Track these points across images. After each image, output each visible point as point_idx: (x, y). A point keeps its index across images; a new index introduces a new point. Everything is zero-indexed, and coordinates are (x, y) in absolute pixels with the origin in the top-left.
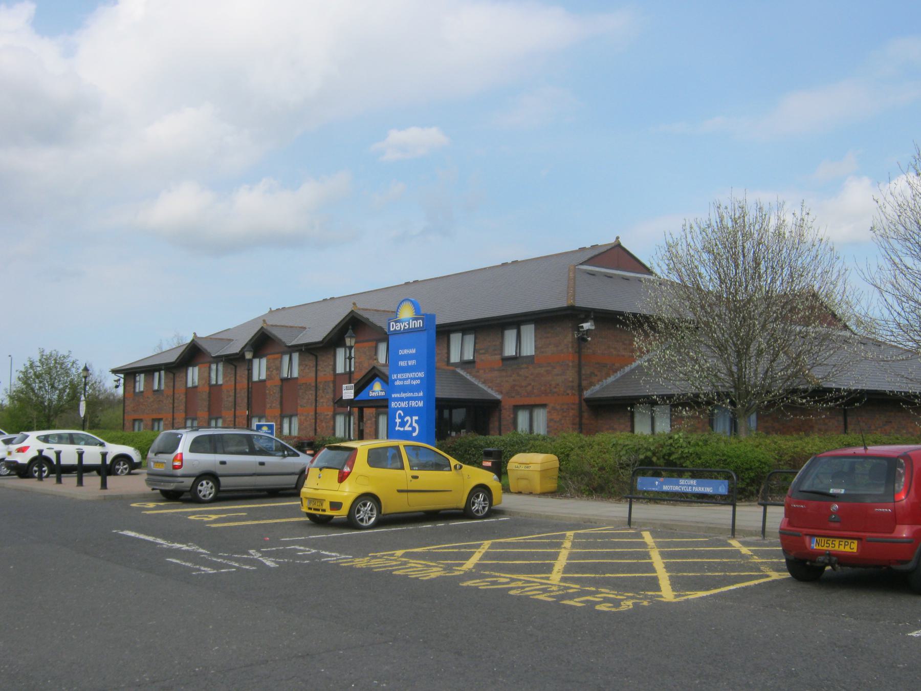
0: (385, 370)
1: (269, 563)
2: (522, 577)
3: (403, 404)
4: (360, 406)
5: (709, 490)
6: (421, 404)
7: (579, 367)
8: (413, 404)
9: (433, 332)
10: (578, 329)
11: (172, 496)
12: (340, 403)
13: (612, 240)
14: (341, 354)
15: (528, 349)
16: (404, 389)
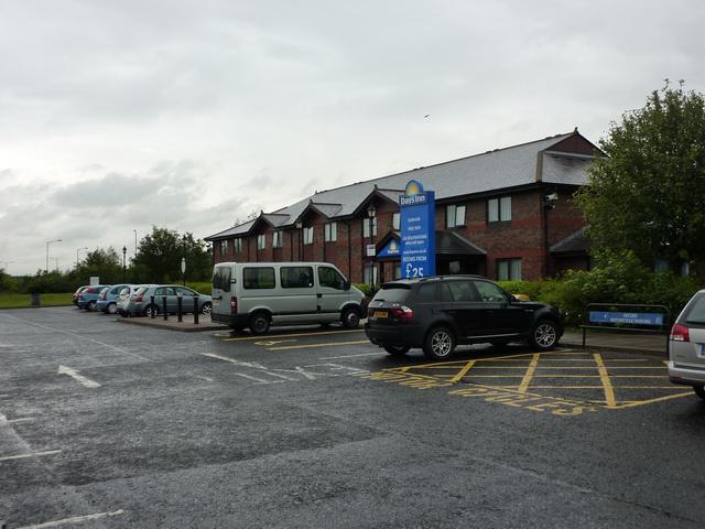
0: (399, 234)
1: (310, 376)
2: (496, 388)
3: (412, 259)
4: (379, 260)
5: (647, 322)
6: (425, 258)
7: (546, 229)
8: (419, 258)
9: (433, 205)
10: (545, 199)
12: (365, 258)
14: (367, 222)
15: (507, 216)
16: (413, 248)
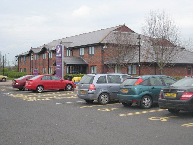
11: (89, 102)
13: (123, 24)
